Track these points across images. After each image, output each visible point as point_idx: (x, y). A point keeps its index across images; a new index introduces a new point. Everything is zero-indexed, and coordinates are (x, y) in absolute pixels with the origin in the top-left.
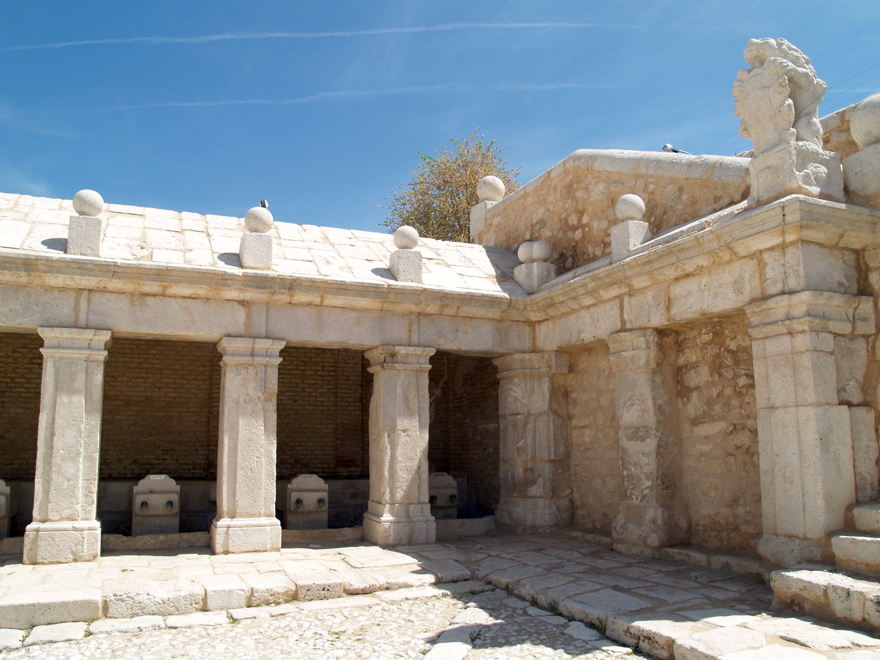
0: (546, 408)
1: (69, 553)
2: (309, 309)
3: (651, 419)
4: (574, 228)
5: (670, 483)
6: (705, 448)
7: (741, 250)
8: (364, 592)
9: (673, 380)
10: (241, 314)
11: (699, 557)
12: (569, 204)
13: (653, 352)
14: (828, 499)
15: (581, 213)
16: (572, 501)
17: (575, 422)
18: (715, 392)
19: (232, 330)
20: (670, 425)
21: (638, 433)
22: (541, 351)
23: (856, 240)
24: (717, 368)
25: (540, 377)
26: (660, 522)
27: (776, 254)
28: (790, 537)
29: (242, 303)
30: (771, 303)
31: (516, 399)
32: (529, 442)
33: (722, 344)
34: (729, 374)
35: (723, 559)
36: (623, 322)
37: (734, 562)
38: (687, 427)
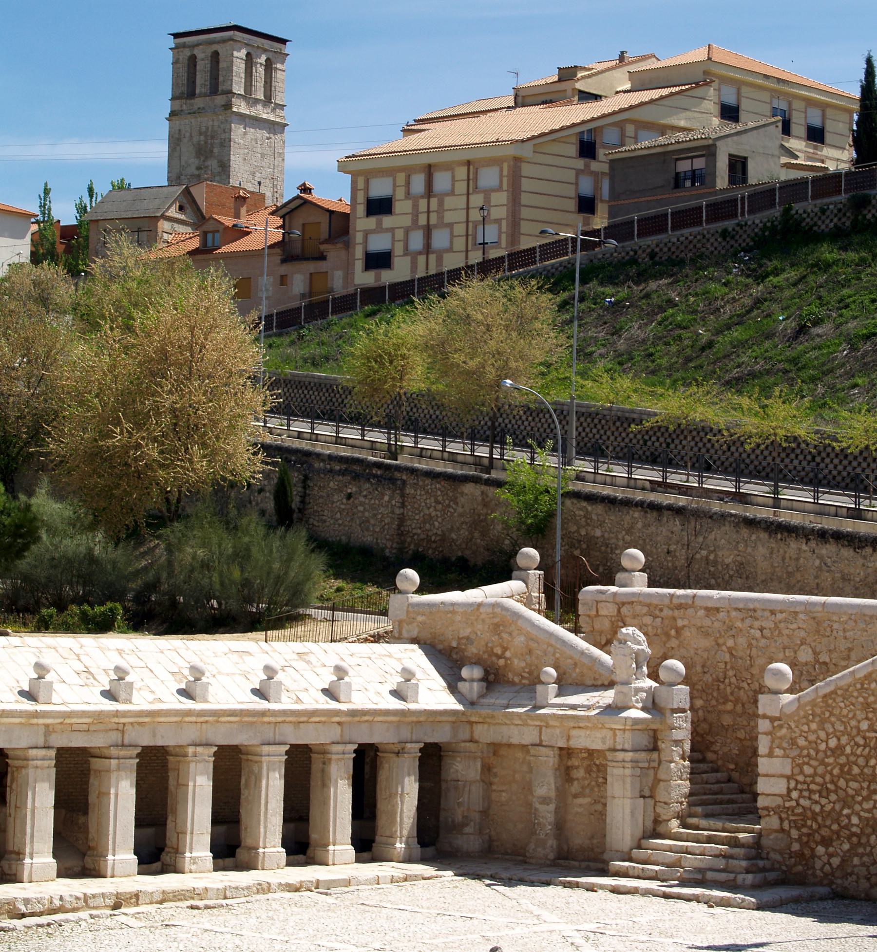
0: (478, 778)
1: (41, 877)
2: (366, 724)
3: (553, 794)
4: (499, 657)
5: (560, 827)
6: (579, 810)
7: (607, 726)
8: (429, 878)
9: (565, 773)
10: (338, 729)
11: (576, 864)
12: (495, 638)
13: (557, 760)
14: (632, 835)
15: (505, 649)
16: (490, 837)
17: (494, 787)
18: (586, 782)
19: (335, 740)
20: (562, 795)
21: (545, 801)
22: (476, 742)
23: (654, 727)
24: (588, 771)
25: (475, 758)
26: (555, 847)
27: (621, 732)
28: (617, 851)
29: (339, 723)
30: (617, 753)
31: (457, 771)
32: (466, 799)
33: (592, 760)
34: (594, 775)
35: (587, 863)
36: (541, 741)
37: (592, 864)
38: (570, 798)
